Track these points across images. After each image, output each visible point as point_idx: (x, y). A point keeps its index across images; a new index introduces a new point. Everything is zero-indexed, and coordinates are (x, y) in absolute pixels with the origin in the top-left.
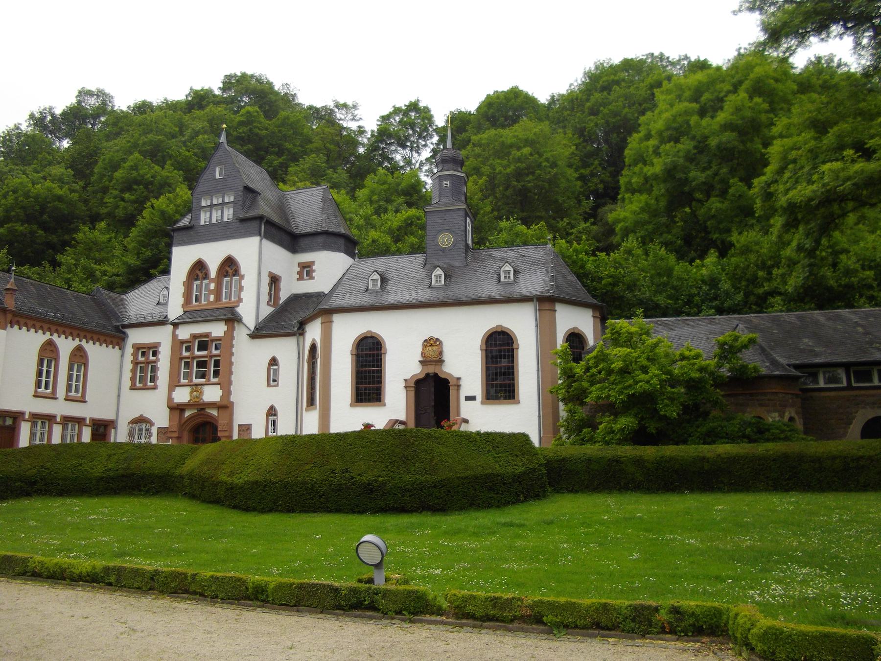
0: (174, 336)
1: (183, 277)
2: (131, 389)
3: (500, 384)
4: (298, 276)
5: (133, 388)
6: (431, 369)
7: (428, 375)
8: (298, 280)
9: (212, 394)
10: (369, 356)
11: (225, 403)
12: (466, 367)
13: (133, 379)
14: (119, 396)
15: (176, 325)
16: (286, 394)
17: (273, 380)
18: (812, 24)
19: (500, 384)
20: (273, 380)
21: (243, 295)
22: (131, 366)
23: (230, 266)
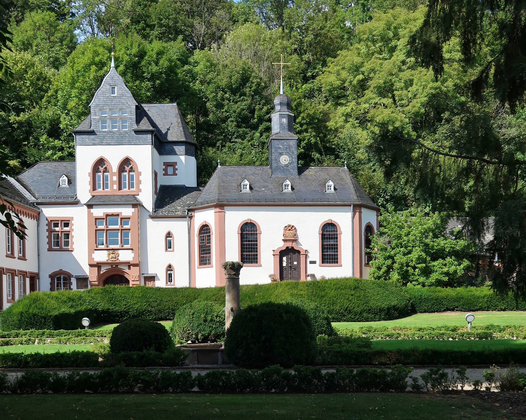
0: (90, 214)
1: (89, 169)
2: (48, 251)
3: (330, 255)
4: (164, 172)
5: (50, 249)
6: (289, 244)
7: (287, 247)
8: (164, 175)
9: (125, 256)
10: (249, 235)
11: (137, 262)
12: (311, 244)
13: (49, 243)
14: (39, 255)
15: (90, 206)
16: (180, 257)
17: (169, 245)
18: (457, 24)
19: (330, 255)
20: (169, 245)
21: (141, 186)
22: (47, 234)
23: (126, 163)
